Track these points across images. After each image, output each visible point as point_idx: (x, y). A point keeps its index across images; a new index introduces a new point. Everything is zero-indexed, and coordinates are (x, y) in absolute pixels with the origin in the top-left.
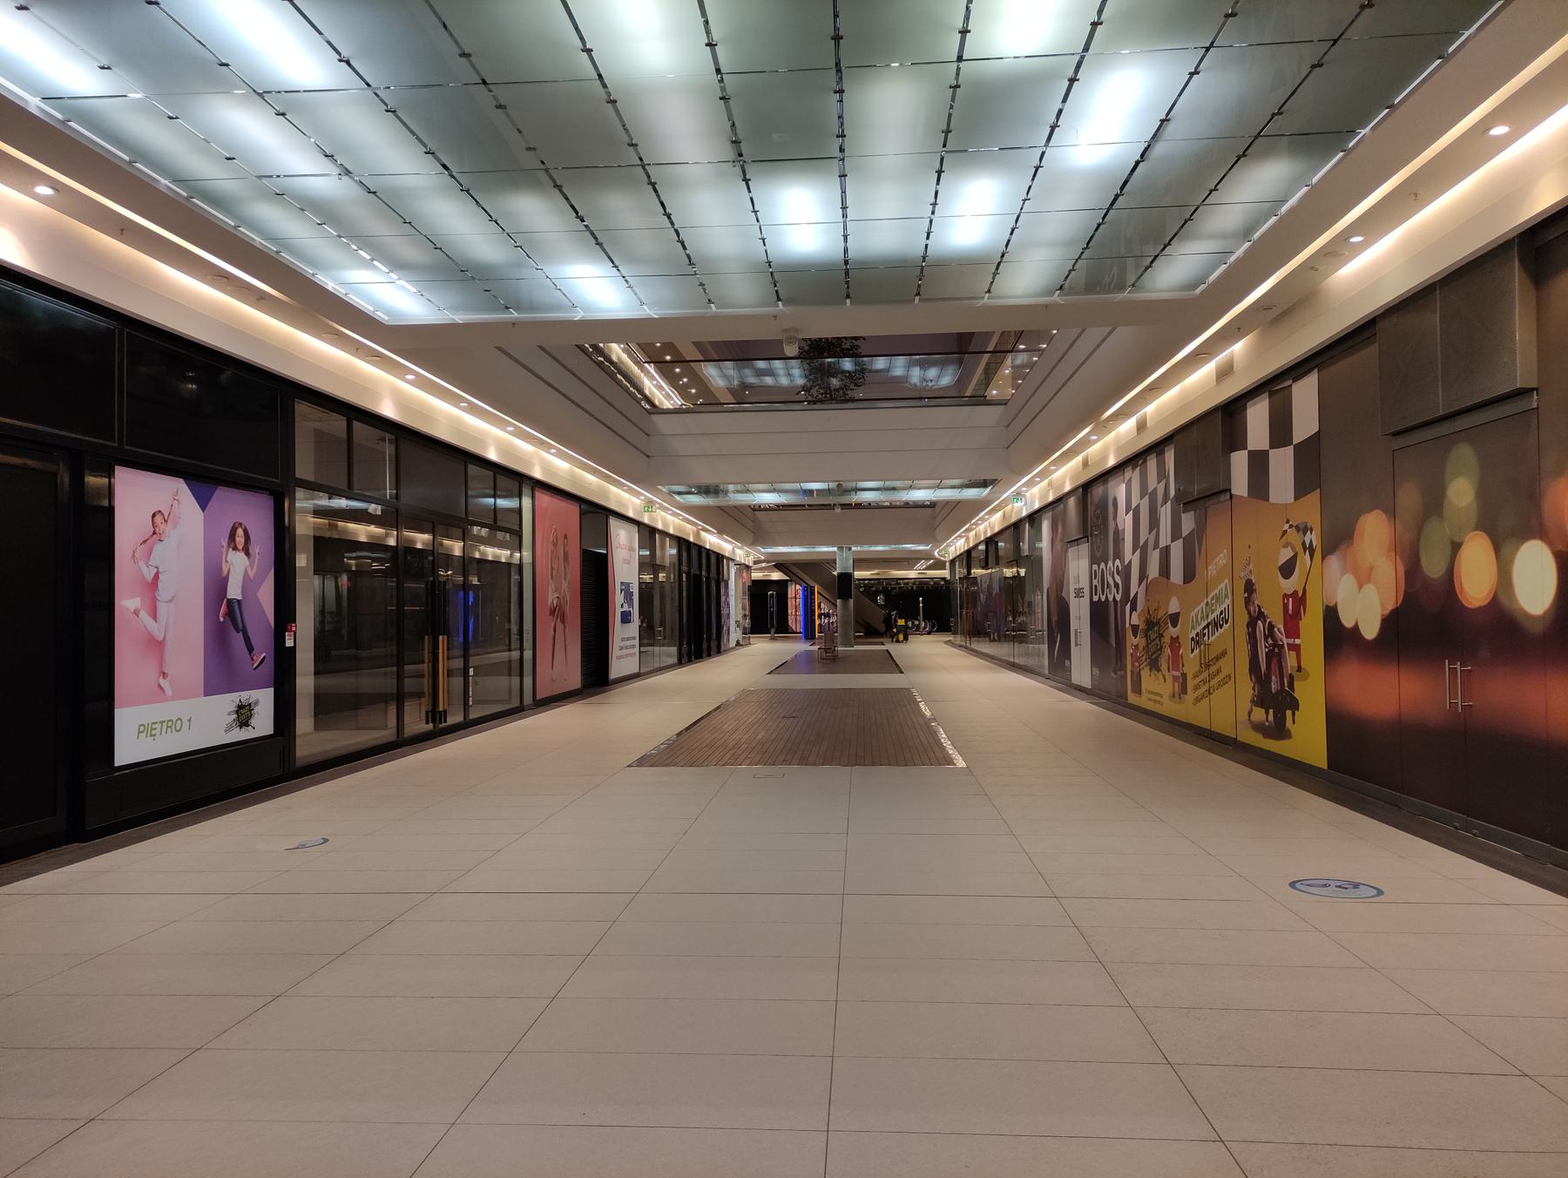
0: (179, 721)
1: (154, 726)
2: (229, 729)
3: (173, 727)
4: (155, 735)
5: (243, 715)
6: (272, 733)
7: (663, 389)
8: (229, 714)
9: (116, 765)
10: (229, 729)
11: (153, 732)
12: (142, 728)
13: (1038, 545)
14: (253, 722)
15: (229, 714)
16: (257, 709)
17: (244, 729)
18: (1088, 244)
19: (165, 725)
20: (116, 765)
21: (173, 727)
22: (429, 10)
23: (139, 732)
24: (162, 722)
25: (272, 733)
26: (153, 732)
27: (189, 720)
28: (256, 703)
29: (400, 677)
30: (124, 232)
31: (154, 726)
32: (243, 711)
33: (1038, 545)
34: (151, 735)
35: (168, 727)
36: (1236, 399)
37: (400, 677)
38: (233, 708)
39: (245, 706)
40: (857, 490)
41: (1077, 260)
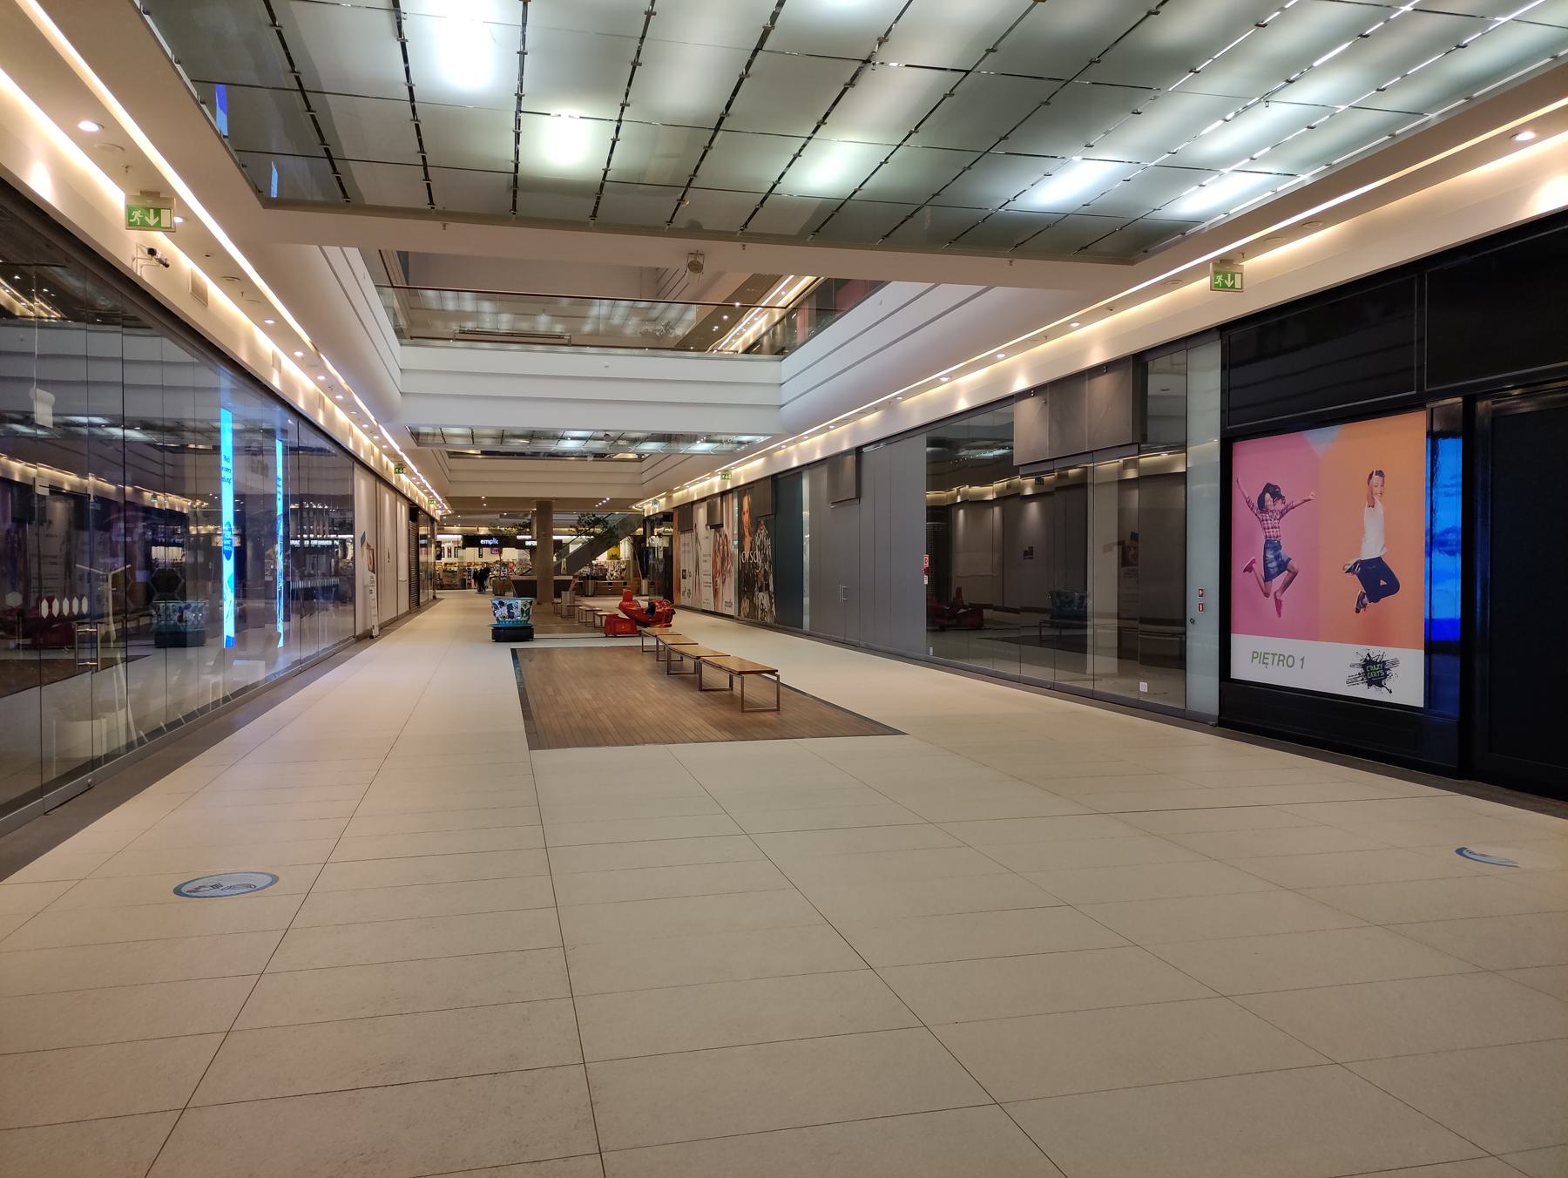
0: (1291, 658)
1: (1266, 656)
2: (1352, 681)
3: (1285, 661)
4: (1267, 664)
5: (1374, 672)
6: (1232, 677)
7: (740, 331)
8: (1352, 666)
9: (1420, 703)
10: (1352, 681)
11: (1266, 661)
12: (1255, 655)
13: (67, 487)
14: (1388, 683)
15: (1352, 666)
16: (1393, 670)
17: (1373, 688)
18: (916, 128)
19: (1276, 657)
20: (1420, 703)
21: (1285, 661)
22: (1141, 24)
23: (1253, 658)
24: (1274, 655)
25: (1232, 677)
26: (1266, 661)
27: (1303, 660)
28: (1395, 663)
29: (1041, 632)
30: (129, 170)
31: (1266, 656)
32: (1373, 668)
33: (67, 487)
34: (1264, 663)
35: (1279, 660)
36: (136, 285)
37: (1041, 632)
38: (1358, 660)
39: (1375, 663)
40: (563, 438)
41: (899, 146)
